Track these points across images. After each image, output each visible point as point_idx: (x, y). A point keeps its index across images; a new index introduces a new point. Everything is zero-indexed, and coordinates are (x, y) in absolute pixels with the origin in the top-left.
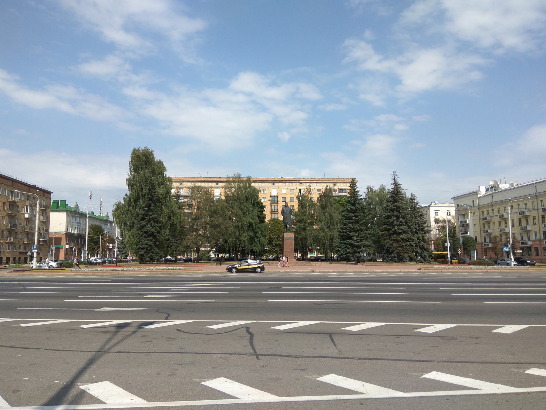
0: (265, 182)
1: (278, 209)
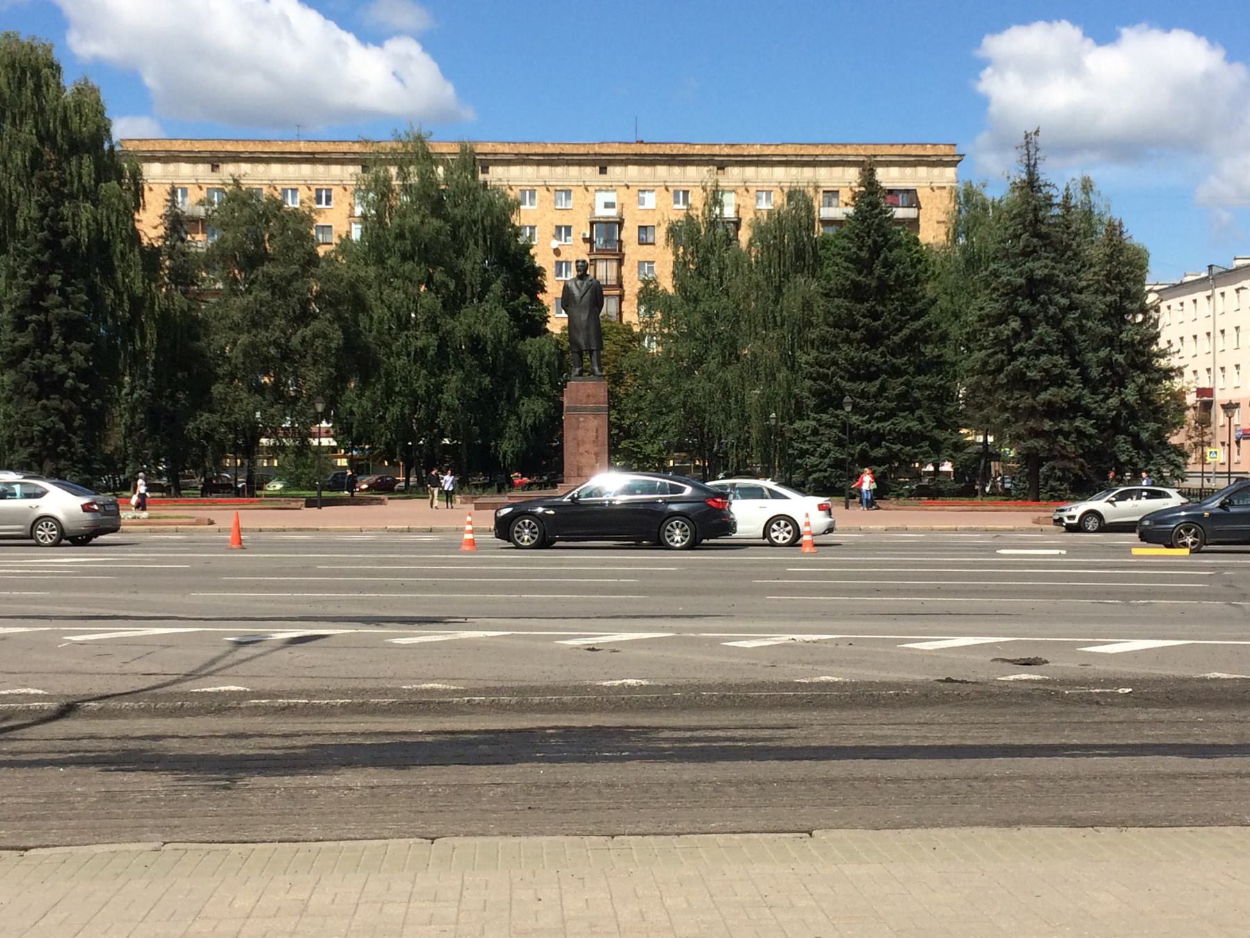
0: (569, 163)
1: (619, 278)
